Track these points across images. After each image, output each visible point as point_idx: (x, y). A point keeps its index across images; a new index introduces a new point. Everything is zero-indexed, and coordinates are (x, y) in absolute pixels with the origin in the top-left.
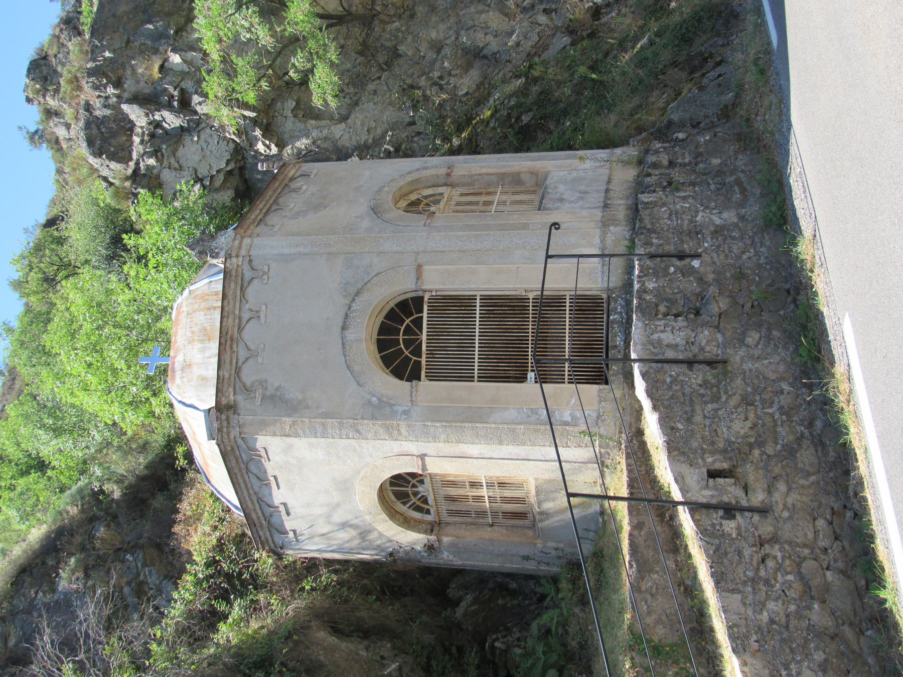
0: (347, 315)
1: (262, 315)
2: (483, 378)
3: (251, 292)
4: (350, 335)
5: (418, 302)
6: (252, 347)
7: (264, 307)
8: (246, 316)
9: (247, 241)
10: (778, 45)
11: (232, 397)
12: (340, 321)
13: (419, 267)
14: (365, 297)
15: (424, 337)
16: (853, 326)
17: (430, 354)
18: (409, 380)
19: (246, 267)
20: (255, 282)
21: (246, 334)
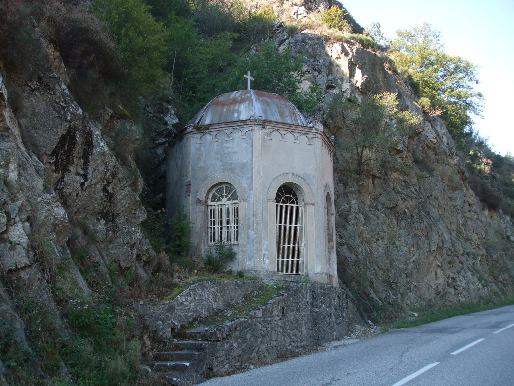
0: (297, 175)
1: (296, 141)
2: (278, 227)
3: (303, 137)
4: (290, 176)
5: (235, 197)
6: (285, 136)
7: (299, 142)
8: (295, 134)
9: (320, 136)
10: (482, 338)
11: (268, 127)
12: (295, 172)
13: (314, 205)
14: (304, 183)
15: (288, 204)
16: (436, 366)
17: (283, 206)
18: (276, 199)
19: (312, 136)
20: (307, 139)
21: (289, 134)
